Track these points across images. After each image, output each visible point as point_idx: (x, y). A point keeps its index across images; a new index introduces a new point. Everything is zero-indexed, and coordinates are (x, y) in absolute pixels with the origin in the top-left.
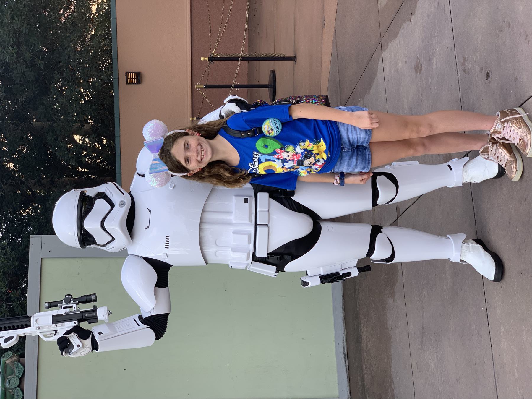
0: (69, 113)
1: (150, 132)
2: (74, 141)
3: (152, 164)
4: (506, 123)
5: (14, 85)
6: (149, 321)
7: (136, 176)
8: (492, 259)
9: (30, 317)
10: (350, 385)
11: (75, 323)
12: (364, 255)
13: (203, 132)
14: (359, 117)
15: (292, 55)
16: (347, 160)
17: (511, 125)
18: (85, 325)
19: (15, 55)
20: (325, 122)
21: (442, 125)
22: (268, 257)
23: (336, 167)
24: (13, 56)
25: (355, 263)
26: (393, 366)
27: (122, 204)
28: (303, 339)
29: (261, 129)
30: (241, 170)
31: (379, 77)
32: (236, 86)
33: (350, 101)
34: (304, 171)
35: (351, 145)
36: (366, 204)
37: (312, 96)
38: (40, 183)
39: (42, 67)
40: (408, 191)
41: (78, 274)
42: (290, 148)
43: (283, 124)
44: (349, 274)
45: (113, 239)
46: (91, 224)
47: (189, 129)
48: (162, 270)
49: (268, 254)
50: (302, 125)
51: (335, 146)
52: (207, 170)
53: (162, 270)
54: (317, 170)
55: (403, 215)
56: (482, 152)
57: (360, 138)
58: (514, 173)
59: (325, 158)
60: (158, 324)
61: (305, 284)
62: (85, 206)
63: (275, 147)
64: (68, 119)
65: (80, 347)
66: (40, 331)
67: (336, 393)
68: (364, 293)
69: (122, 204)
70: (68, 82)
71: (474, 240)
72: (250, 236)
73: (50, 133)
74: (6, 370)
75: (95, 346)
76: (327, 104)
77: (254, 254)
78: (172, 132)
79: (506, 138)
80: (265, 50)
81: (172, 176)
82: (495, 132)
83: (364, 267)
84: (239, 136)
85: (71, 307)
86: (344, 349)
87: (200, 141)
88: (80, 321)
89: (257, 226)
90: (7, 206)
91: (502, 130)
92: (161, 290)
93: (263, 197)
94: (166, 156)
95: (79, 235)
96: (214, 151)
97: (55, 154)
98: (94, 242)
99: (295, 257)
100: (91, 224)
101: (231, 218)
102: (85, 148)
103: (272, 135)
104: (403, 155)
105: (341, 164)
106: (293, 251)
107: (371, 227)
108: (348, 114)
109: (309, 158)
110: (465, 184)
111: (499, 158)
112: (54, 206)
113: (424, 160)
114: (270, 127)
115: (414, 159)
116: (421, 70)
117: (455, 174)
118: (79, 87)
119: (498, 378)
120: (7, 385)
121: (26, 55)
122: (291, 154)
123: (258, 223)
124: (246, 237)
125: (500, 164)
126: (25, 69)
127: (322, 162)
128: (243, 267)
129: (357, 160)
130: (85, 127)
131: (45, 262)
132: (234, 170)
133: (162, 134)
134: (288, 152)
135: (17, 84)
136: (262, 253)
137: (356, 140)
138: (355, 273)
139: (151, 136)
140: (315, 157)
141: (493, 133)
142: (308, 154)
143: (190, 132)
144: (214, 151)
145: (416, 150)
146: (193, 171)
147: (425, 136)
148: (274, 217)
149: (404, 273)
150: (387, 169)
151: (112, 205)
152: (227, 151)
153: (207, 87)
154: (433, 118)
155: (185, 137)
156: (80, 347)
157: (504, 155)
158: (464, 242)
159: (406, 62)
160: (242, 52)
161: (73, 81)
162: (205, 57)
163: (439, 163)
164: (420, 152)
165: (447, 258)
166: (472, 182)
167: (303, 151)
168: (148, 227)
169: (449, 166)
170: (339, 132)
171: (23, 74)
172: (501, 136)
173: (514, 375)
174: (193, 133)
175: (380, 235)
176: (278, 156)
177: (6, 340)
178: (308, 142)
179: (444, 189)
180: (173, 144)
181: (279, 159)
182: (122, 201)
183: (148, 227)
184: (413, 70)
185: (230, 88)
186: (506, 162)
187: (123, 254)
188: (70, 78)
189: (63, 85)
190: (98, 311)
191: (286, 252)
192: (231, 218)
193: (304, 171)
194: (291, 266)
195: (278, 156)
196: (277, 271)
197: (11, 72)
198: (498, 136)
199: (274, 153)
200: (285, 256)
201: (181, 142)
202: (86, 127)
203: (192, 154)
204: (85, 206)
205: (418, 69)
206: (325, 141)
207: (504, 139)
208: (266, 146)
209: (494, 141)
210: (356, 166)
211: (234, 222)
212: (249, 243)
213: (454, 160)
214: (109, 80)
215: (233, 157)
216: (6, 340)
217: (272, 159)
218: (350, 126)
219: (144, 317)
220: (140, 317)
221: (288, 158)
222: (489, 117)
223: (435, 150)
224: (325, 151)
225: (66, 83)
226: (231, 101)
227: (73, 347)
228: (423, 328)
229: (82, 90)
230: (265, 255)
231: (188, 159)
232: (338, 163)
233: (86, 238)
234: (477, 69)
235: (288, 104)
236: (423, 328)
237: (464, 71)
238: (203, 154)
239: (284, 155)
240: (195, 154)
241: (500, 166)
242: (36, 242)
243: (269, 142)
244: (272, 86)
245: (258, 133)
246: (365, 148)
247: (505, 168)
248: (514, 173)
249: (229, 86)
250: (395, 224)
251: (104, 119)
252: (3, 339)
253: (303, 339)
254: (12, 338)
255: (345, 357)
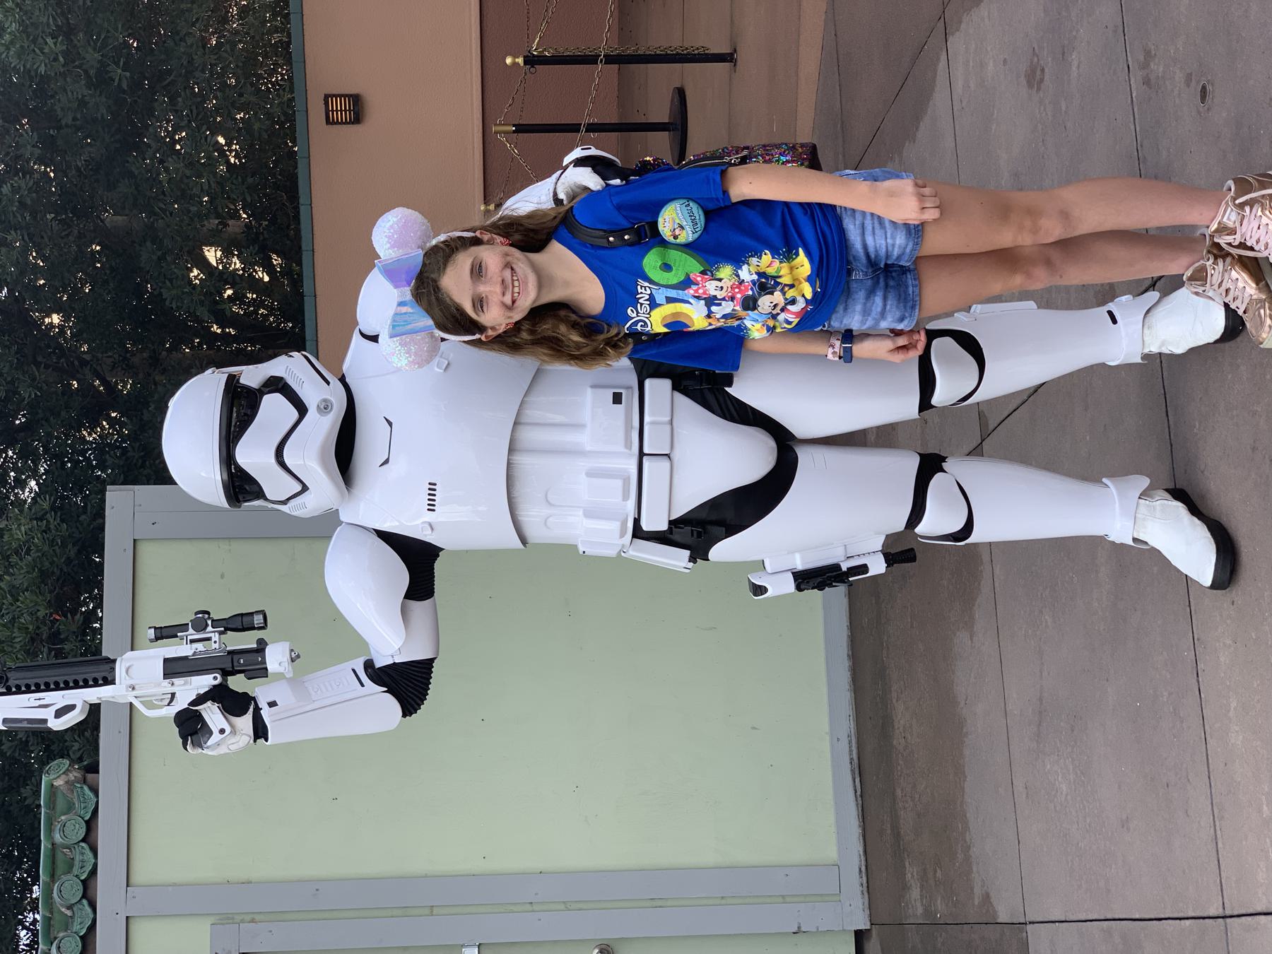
0: (191, 197)
1: (389, 237)
2: (203, 264)
3: (396, 314)
4: (1247, 209)
5: (59, 128)
6: (389, 675)
7: (356, 339)
8: (1209, 535)
9: (114, 661)
10: (864, 836)
11: (215, 678)
12: (899, 524)
13: (517, 237)
14: (891, 194)
15: (725, 49)
16: (862, 301)
17: (1260, 213)
18: (238, 683)
19: (61, 59)
20: (808, 207)
21: (1095, 211)
22: (670, 528)
23: (834, 317)
24: (56, 59)
25: (878, 543)
26: (967, 790)
27: (325, 407)
28: (754, 728)
29: (654, 225)
30: (609, 326)
31: (940, 99)
32: (592, 128)
33: (871, 158)
34: (758, 326)
35: (872, 263)
36: (904, 406)
37: (778, 146)
38: (126, 366)
39: (125, 86)
40: (1009, 374)
41: (222, 576)
42: (726, 272)
43: (708, 214)
44: (863, 569)
45: (305, 488)
46: (253, 455)
47: (484, 229)
48: (418, 561)
49: (670, 522)
50: (753, 216)
51: (832, 263)
52: (526, 326)
53: (418, 561)
54: (789, 323)
55: (1000, 431)
56: (1190, 279)
57: (893, 245)
58: (1267, 329)
59: (809, 296)
60: (407, 683)
61: (759, 590)
62: (240, 409)
63: (688, 269)
64: (189, 211)
65: (227, 734)
66: (135, 693)
67: (831, 853)
68: (899, 614)
69: (325, 407)
70: (190, 122)
71: (1167, 490)
72: (626, 481)
73: (148, 244)
74: (54, 803)
75: (260, 731)
76: (814, 164)
77: (637, 522)
78: (442, 238)
79: (1249, 244)
80: (658, 38)
81: (443, 340)
82: (1223, 229)
83: (901, 552)
84: (603, 242)
85: (209, 639)
86: (851, 751)
87: (509, 258)
88: (226, 673)
89: (645, 458)
90: (47, 420)
91: (1237, 225)
92: (418, 607)
93: (658, 388)
94: (429, 294)
95: (225, 477)
96: (543, 280)
97: (161, 294)
98: (259, 494)
99: (733, 529)
100: (253, 455)
101: (583, 439)
102: (230, 280)
103: (681, 240)
104: (997, 287)
105: (846, 309)
106: (729, 515)
107: (917, 459)
108: (863, 187)
109: (772, 293)
110: (1146, 357)
111: (1231, 293)
112: (167, 407)
113: (1047, 300)
114: (677, 220)
115: (1023, 296)
116: (1042, 80)
117: (1123, 334)
118: (214, 134)
119: (1222, 818)
120: (58, 838)
121: (88, 56)
122: (727, 283)
123: (646, 451)
124: (619, 483)
125: (1233, 306)
126: (86, 92)
127: (801, 304)
128: (612, 553)
129: (885, 299)
130: (230, 229)
131: (144, 548)
132: (590, 326)
133: (420, 242)
134: (720, 280)
135: (67, 126)
136: (655, 521)
137: (883, 252)
138: (878, 566)
139: (392, 247)
140: (784, 294)
141: (1216, 231)
142: (766, 284)
143: (486, 237)
144: (543, 280)
145: (1028, 275)
146: (493, 328)
147: (1052, 240)
148: (683, 431)
149: (997, 571)
150: (960, 322)
151: (302, 409)
152: (575, 278)
153: (521, 129)
154: (1070, 195)
155: (474, 249)
156: (227, 734)
157: (1244, 287)
158: (1144, 495)
159: (1005, 61)
160: (605, 43)
161: (202, 122)
162: (515, 57)
163: (1085, 305)
164: (1041, 279)
165: (1102, 534)
166: (1165, 350)
167: (755, 277)
168: (387, 462)
169: (1110, 313)
170: (842, 232)
171: (82, 103)
172: (1237, 239)
173: (1260, 811)
174: (493, 239)
175: (938, 477)
176: (696, 291)
177: (59, 713)
178: (767, 257)
179: (1098, 371)
180: (445, 269)
181: (698, 298)
182: (325, 400)
183: (387, 462)
184: (1023, 80)
185: (577, 131)
186: (1246, 301)
187: (327, 524)
188: (195, 111)
189: (177, 129)
190: (269, 651)
191: (713, 517)
192: (583, 439)
193: (758, 326)
194: (724, 550)
195: (696, 291)
196: (693, 559)
197: (52, 97)
198: (1229, 239)
199: (687, 283)
200: (709, 527)
201: (463, 261)
202: (234, 227)
203: (490, 289)
204: (240, 409)
205: (1034, 78)
206: (809, 254)
207: (1242, 246)
208: (667, 267)
209: (1219, 252)
210: (883, 315)
211: (588, 448)
212: (626, 497)
213: (1124, 298)
214: (285, 114)
215: (589, 292)
216: (59, 713)
217: (677, 300)
218: (869, 217)
219: (378, 664)
220: (369, 665)
221: (720, 295)
222: (1210, 193)
223: (1077, 275)
224: (809, 279)
225: (183, 124)
226: (579, 162)
227: (211, 733)
228: (1041, 699)
229: (221, 140)
230: (663, 526)
231: (481, 301)
232: (840, 308)
233: (240, 486)
234: (1179, 76)
235: (719, 166)
236: (1041, 699)
237: (1147, 82)
238: (516, 290)
239: (711, 288)
240: (498, 289)
241: (1230, 312)
242: (123, 505)
243: (675, 256)
244: (678, 126)
245: (649, 236)
246: (904, 271)
247: (1244, 317)
248: (1267, 329)
249: (574, 128)
250: (976, 452)
251: (275, 212)
252: (53, 710)
253: (754, 728)
254: (72, 707)
255: (853, 771)
